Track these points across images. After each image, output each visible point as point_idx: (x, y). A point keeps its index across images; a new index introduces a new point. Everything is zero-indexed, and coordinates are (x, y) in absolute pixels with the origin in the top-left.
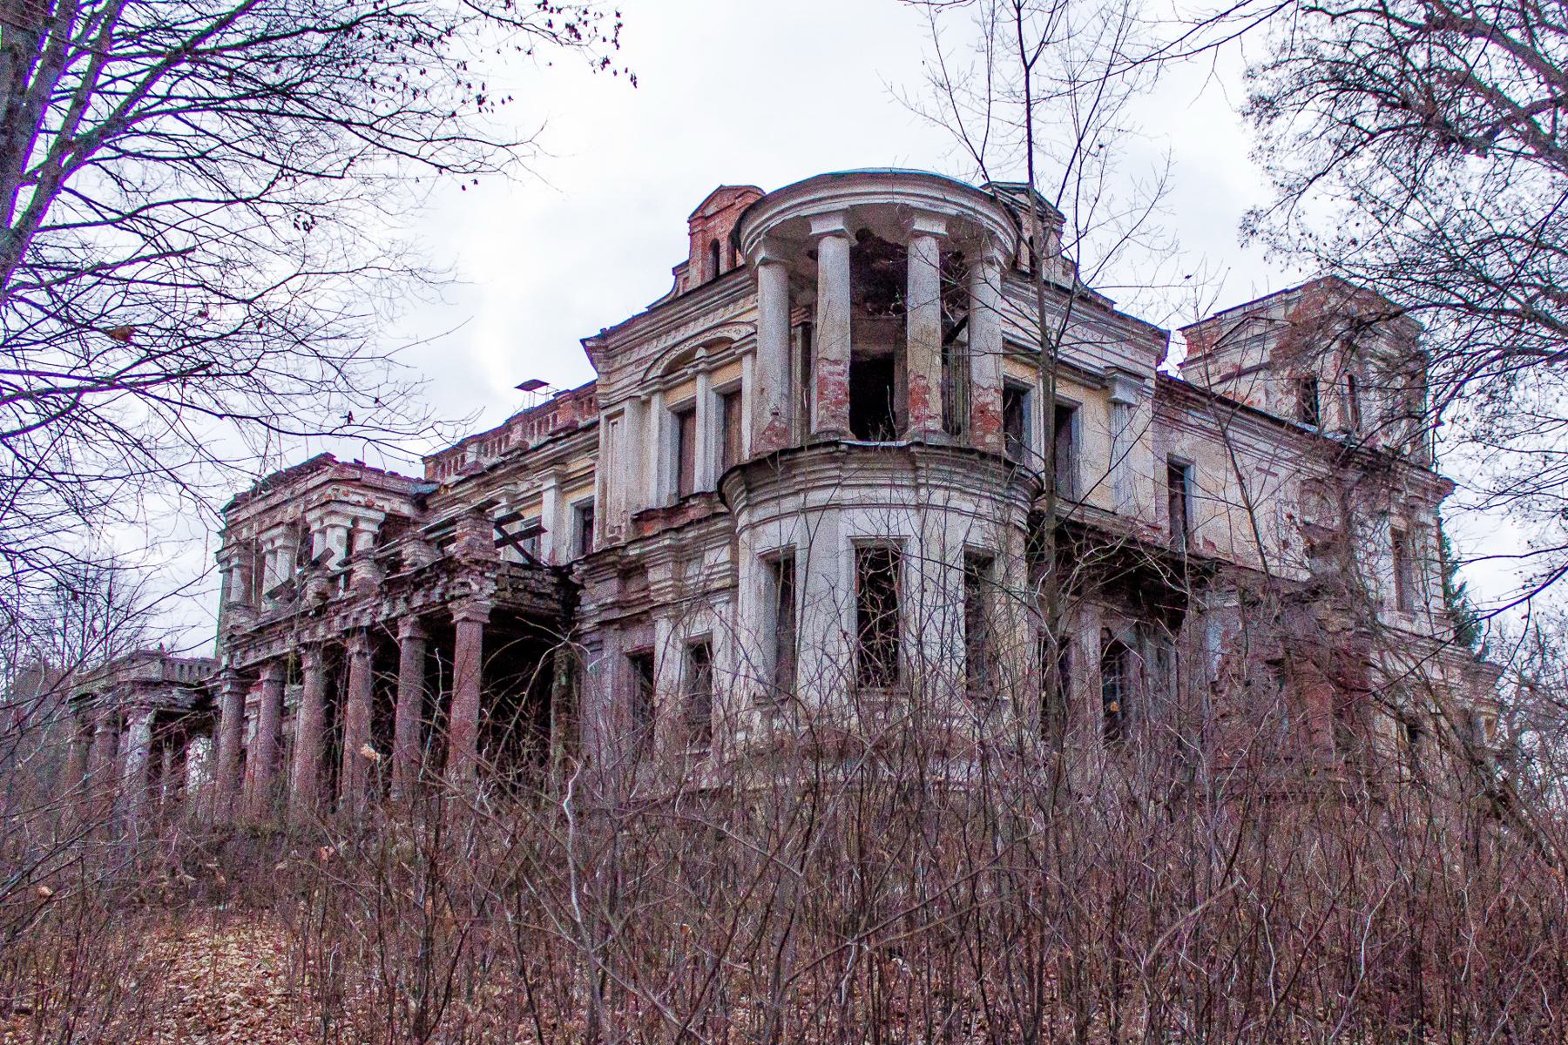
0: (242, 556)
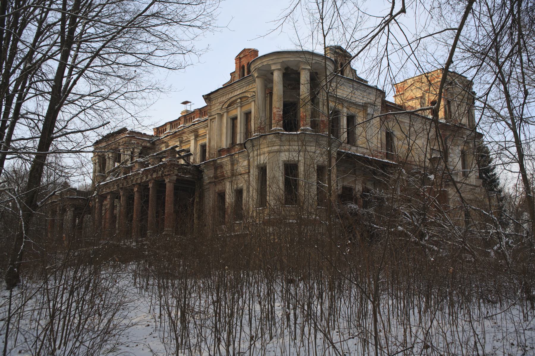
0: (101, 162)
